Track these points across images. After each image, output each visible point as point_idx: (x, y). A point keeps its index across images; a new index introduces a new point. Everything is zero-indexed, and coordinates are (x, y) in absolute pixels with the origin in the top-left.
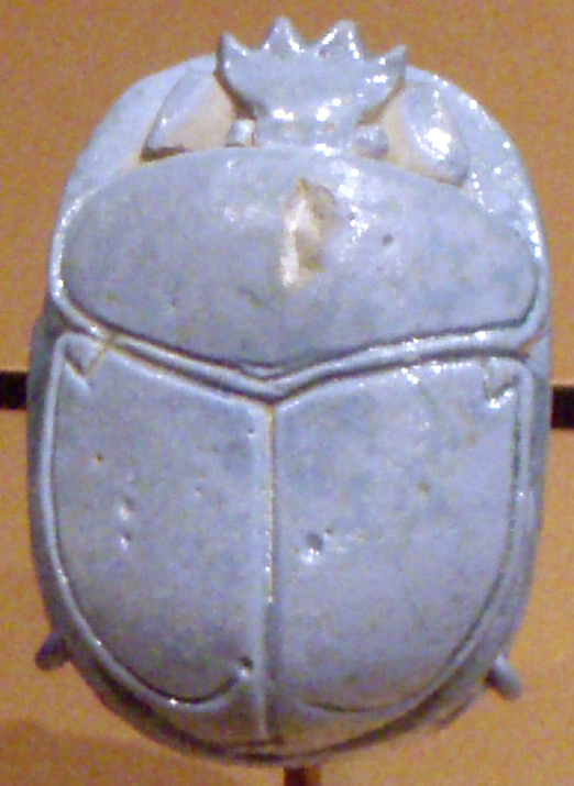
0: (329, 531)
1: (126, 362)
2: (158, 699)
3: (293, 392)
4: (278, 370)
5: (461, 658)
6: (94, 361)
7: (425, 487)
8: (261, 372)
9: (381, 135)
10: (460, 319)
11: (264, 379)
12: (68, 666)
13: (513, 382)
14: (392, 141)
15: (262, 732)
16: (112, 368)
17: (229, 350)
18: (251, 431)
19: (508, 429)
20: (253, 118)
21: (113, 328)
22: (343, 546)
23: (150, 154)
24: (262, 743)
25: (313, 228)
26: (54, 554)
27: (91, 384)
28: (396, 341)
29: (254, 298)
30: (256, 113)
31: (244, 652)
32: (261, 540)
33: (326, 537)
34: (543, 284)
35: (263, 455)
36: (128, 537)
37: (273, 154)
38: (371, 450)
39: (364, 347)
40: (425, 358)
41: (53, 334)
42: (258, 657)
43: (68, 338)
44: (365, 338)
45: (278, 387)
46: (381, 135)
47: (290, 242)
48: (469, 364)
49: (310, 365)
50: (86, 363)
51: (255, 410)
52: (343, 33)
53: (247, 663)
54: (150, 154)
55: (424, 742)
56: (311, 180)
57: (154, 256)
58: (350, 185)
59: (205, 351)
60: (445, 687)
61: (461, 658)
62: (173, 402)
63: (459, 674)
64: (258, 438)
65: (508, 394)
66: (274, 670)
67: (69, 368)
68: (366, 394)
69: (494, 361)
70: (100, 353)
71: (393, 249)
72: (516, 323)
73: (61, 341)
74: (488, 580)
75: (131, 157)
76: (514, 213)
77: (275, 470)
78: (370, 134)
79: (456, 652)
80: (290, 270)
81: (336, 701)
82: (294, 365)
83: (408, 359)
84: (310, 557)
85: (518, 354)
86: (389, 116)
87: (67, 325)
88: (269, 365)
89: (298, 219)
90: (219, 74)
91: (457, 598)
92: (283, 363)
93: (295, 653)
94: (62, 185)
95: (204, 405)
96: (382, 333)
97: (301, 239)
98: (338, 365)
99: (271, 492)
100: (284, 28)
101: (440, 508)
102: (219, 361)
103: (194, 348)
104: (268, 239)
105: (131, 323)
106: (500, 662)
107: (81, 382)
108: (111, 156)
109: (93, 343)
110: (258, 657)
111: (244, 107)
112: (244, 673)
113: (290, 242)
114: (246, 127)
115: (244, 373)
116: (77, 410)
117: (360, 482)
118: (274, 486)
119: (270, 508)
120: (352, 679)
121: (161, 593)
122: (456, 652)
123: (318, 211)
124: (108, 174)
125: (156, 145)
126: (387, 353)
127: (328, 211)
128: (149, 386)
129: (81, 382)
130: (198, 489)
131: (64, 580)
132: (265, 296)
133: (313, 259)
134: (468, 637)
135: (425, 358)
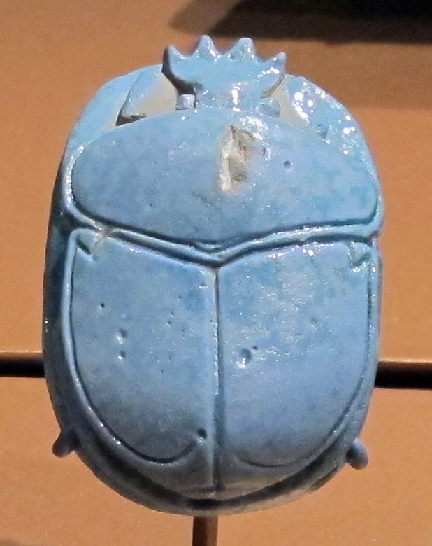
0: (255, 348)
1: (121, 244)
4: (218, 246)
7: (314, 320)
8: (212, 247)
11: (209, 252)
12: (74, 453)
15: (210, 483)
16: (111, 249)
18: (203, 285)
19: (364, 287)
20: (192, 93)
21: (109, 223)
23: (121, 120)
24: (210, 490)
26: (73, 368)
27: (95, 258)
28: (292, 228)
29: (204, 199)
31: (200, 426)
33: (253, 352)
36: (123, 354)
38: (281, 297)
40: (312, 239)
41: (65, 235)
44: (274, 225)
45: (220, 256)
46: (276, 103)
47: (225, 164)
49: (239, 242)
50: (91, 247)
51: (204, 272)
53: (202, 433)
54: (121, 120)
55: (302, 501)
56: (236, 125)
62: (150, 267)
63: (331, 449)
64: (208, 289)
65: (365, 264)
72: (366, 221)
73: (74, 233)
79: (336, 427)
80: (226, 184)
81: (259, 460)
82: (230, 242)
83: (302, 240)
84: (242, 365)
85: (367, 241)
86: (278, 93)
87: (76, 224)
88: (213, 243)
89: (229, 150)
90: (167, 72)
92: (222, 241)
93: (232, 427)
94: (70, 135)
95: (171, 267)
96: (285, 223)
99: (216, 324)
102: (180, 244)
104: (212, 163)
105: (124, 220)
106: (357, 442)
109: (96, 236)
110: (210, 430)
111: (183, 88)
112: (200, 440)
114: (189, 98)
115: (197, 248)
119: (216, 334)
120: (270, 444)
122: (336, 427)
123: (242, 146)
125: (128, 113)
126: (287, 235)
127: (243, 140)
131: (79, 385)
132: (211, 199)
134: (341, 419)
135: (312, 239)
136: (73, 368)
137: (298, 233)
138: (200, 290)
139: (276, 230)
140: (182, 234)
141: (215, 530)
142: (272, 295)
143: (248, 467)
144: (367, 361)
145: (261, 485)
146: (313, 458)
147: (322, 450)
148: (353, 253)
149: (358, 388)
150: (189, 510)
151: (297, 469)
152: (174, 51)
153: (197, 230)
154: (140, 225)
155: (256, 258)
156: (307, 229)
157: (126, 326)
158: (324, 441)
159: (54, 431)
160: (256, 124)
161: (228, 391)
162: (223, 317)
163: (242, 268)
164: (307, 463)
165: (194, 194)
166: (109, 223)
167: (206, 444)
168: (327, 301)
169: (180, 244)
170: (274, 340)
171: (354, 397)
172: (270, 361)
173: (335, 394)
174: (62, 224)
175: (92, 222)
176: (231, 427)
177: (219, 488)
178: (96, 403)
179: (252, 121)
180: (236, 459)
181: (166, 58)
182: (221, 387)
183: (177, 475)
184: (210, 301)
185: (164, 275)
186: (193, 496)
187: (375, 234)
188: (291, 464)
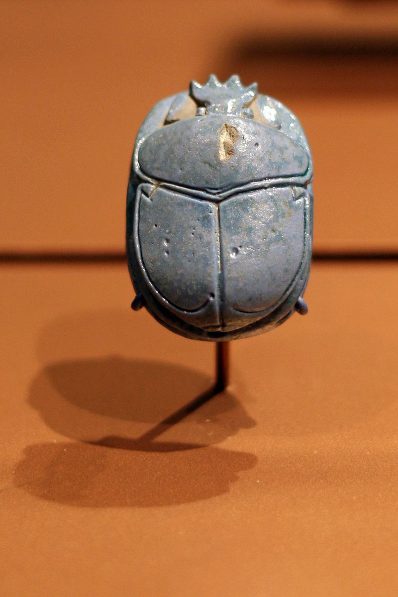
0: (240, 247)
2: (182, 312)
3: (226, 198)
5: (288, 293)
6: (152, 192)
7: (273, 231)
8: (214, 191)
9: (251, 111)
11: (214, 194)
13: (302, 195)
14: (255, 114)
16: (160, 194)
19: (302, 211)
20: (206, 107)
21: (159, 180)
22: (245, 251)
23: (167, 122)
24: (218, 327)
27: (151, 200)
28: (261, 180)
30: (206, 105)
32: (216, 251)
33: (239, 249)
34: (311, 162)
35: (216, 222)
36: (168, 253)
37: (213, 117)
39: (249, 182)
42: (217, 293)
43: (144, 184)
44: (250, 178)
46: (251, 111)
48: (287, 188)
49: (231, 189)
50: (149, 193)
51: (212, 206)
52: (236, 79)
53: (213, 295)
56: (228, 124)
57: (173, 152)
58: (242, 127)
59: (193, 185)
60: (281, 306)
61: (288, 293)
62: (181, 204)
64: (214, 215)
66: (222, 297)
67: (143, 195)
68: (251, 198)
69: (296, 188)
70: (154, 189)
71: (259, 148)
73: (140, 186)
75: (160, 125)
76: (298, 140)
77: (220, 226)
78: (248, 111)
79: (287, 289)
80: (223, 155)
83: (266, 186)
84: (233, 256)
85: (304, 185)
89: (224, 138)
92: (221, 188)
95: (193, 204)
98: (242, 188)
99: (219, 234)
100: (214, 78)
101: (279, 239)
103: (188, 183)
104: (214, 145)
105: (167, 178)
106: (300, 299)
107: (148, 199)
108: (154, 124)
109: (152, 187)
110: (217, 293)
111: (200, 104)
112: (211, 299)
114: (203, 109)
116: (148, 210)
117: (250, 230)
118: (220, 232)
121: (180, 271)
122: (287, 289)
123: (231, 135)
125: (170, 119)
126: (258, 184)
127: (233, 133)
128: (172, 198)
129: (148, 199)
130: (193, 234)
131: (138, 246)
132: (215, 165)
133: (230, 152)
134: (291, 285)
138: (209, 216)
140: (200, 185)
143: (238, 313)
144: (304, 253)
147: (280, 303)
148: (295, 191)
153: (207, 182)
154: (176, 180)
155: (240, 197)
157: (168, 236)
159: (132, 295)
161: (226, 272)
164: (272, 310)
165: (205, 163)
166: (159, 180)
167: (215, 300)
172: (249, 254)
173: (286, 271)
174: (135, 181)
176: (228, 290)
177: (223, 325)
178: (153, 279)
180: (232, 309)
181: (191, 87)
182: (222, 269)
184: (215, 222)
185: (190, 207)
186: (210, 330)
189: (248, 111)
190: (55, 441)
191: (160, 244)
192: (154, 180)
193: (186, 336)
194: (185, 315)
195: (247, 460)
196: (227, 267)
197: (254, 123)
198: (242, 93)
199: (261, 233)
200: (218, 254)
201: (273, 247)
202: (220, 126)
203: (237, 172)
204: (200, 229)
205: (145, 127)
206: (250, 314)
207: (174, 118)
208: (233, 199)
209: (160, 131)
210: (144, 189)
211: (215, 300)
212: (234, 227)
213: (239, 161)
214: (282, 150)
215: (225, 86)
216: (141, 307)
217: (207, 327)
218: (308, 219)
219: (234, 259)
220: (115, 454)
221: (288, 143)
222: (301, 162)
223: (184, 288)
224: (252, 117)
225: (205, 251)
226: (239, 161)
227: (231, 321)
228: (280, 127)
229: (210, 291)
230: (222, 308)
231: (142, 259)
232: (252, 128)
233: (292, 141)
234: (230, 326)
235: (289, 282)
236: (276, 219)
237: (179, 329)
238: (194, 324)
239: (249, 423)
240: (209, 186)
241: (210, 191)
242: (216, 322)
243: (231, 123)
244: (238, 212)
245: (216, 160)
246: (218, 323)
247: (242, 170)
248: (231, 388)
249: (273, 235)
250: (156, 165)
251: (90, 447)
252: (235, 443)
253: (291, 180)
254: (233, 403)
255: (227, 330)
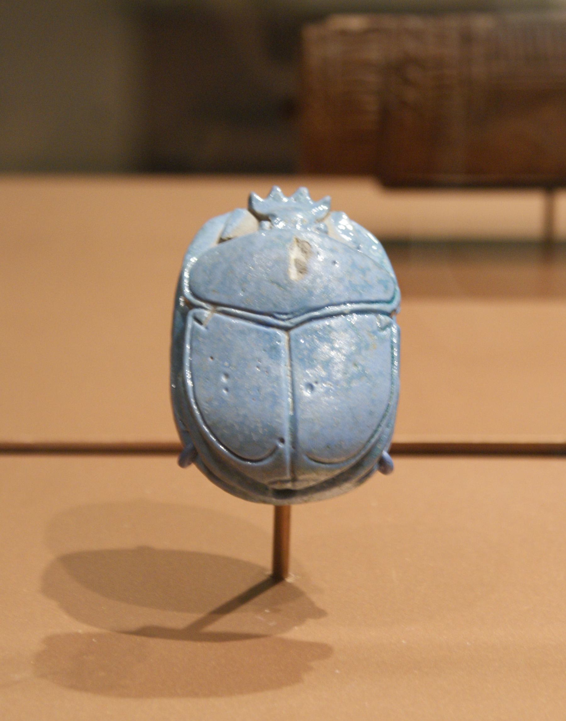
0: (316, 383)
3: (297, 325)
4: (290, 316)
5: (373, 440)
7: (355, 365)
8: (285, 317)
9: (326, 226)
10: (367, 297)
16: (216, 320)
17: (269, 307)
19: (388, 344)
21: (215, 304)
23: (222, 240)
24: (286, 481)
25: (302, 257)
26: (192, 401)
27: (207, 328)
28: (338, 304)
29: (279, 285)
32: (286, 387)
33: (315, 385)
36: (227, 389)
40: (352, 312)
42: (287, 438)
43: (196, 311)
44: (327, 301)
45: (291, 323)
46: (326, 226)
47: (292, 263)
49: (303, 314)
50: (203, 320)
51: (279, 333)
53: (282, 441)
56: (299, 238)
59: (258, 308)
61: (373, 440)
62: (243, 332)
63: (369, 453)
65: (388, 329)
66: (295, 443)
67: (196, 324)
69: (382, 317)
72: (389, 302)
74: (384, 407)
75: (213, 244)
78: (322, 226)
79: (372, 436)
80: (293, 274)
82: (297, 313)
83: (346, 312)
84: (307, 393)
85: (389, 314)
86: (327, 222)
89: (295, 254)
91: (371, 413)
92: (292, 313)
95: (258, 331)
96: (335, 300)
97: (297, 262)
98: (317, 313)
102: (265, 316)
104: (283, 262)
105: (224, 300)
107: (202, 328)
109: (207, 313)
110: (287, 438)
111: (260, 218)
112: (281, 445)
113: (292, 263)
114: (266, 224)
116: (201, 339)
117: (327, 364)
118: (291, 366)
122: (372, 436)
123: (304, 251)
124: (206, 248)
127: (305, 248)
131: (197, 412)
132: (283, 284)
133: (303, 270)
134: (376, 431)
135: (352, 312)
136: (192, 401)
137: (343, 308)
138: (277, 345)
139: (327, 306)
140: (265, 309)
141: (289, 517)
142: (325, 348)
143: (314, 463)
144: (391, 393)
145: (323, 477)
146: (358, 458)
147: (363, 453)
148: (380, 321)
149: (387, 411)
150: (274, 500)
151: (346, 467)
152: (257, 197)
153: (275, 305)
154: (237, 303)
155: (316, 325)
156: (348, 304)
157: (227, 371)
158: (364, 447)
160: (314, 239)
161: (299, 412)
162: (294, 363)
163: (306, 332)
164: (353, 462)
165: (273, 282)
166: (215, 304)
167: (285, 447)
168: (364, 352)
169: (265, 316)
170: (329, 378)
171: (384, 416)
172: (327, 392)
174: (182, 312)
175: (203, 304)
176: (302, 434)
177: (294, 480)
178: (209, 423)
179: (310, 235)
180: (305, 458)
181: (250, 200)
182: (294, 409)
183: (265, 471)
184: (284, 354)
185: (254, 336)
186: (277, 487)
187: (394, 311)
188: (342, 462)
189: (322, 226)
190: (80, 631)
191: (218, 379)
192: (208, 305)
193: (245, 497)
194: (249, 467)
195: (323, 651)
196: (300, 406)
197: (331, 239)
198: (313, 207)
199: (341, 367)
200: (288, 391)
201: (355, 384)
202: (289, 240)
203: (311, 293)
204: (266, 361)
205: (195, 246)
206: (328, 466)
207: (231, 236)
208: (307, 326)
209: (212, 251)
210: (198, 316)
211: (285, 447)
212: (309, 360)
213: (313, 281)
214: (364, 271)
215: (292, 199)
216: (189, 464)
217: (275, 483)
218: (396, 354)
219: (308, 397)
220: (157, 645)
221: (370, 264)
222: (386, 287)
223: (247, 432)
224: (326, 232)
225: (274, 387)
226: (313, 281)
227: (303, 474)
228: (359, 248)
229: (279, 436)
230: (294, 456)
231: (195, 398)
232: (327, 243)
233: (375, 263)
234: (303, 481)
235: (374, 428)
236: (359, 350)
237: (239, 488)
238: (258, 479)
239: (319, 613)
240: (278, 310)
241: (277, 316)
242: (285, 474)
243: (305, 236)
244: (313, 340)
245: (286, 280)
246: (288, 477)
247: (318, 292)
248: (290, 580)
249: (354, 369)
250: (211, 287)
251: (124, 636)
252: (303, 632)
253: (375, 306)
254: (296, 593)
255: (299, 486)
